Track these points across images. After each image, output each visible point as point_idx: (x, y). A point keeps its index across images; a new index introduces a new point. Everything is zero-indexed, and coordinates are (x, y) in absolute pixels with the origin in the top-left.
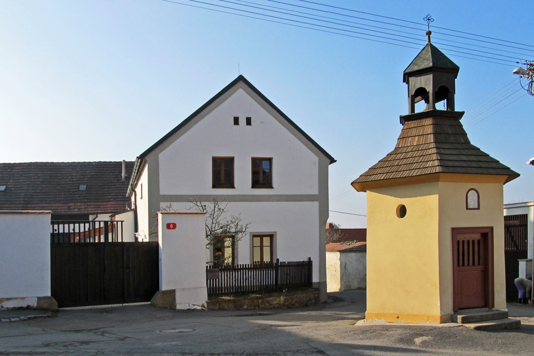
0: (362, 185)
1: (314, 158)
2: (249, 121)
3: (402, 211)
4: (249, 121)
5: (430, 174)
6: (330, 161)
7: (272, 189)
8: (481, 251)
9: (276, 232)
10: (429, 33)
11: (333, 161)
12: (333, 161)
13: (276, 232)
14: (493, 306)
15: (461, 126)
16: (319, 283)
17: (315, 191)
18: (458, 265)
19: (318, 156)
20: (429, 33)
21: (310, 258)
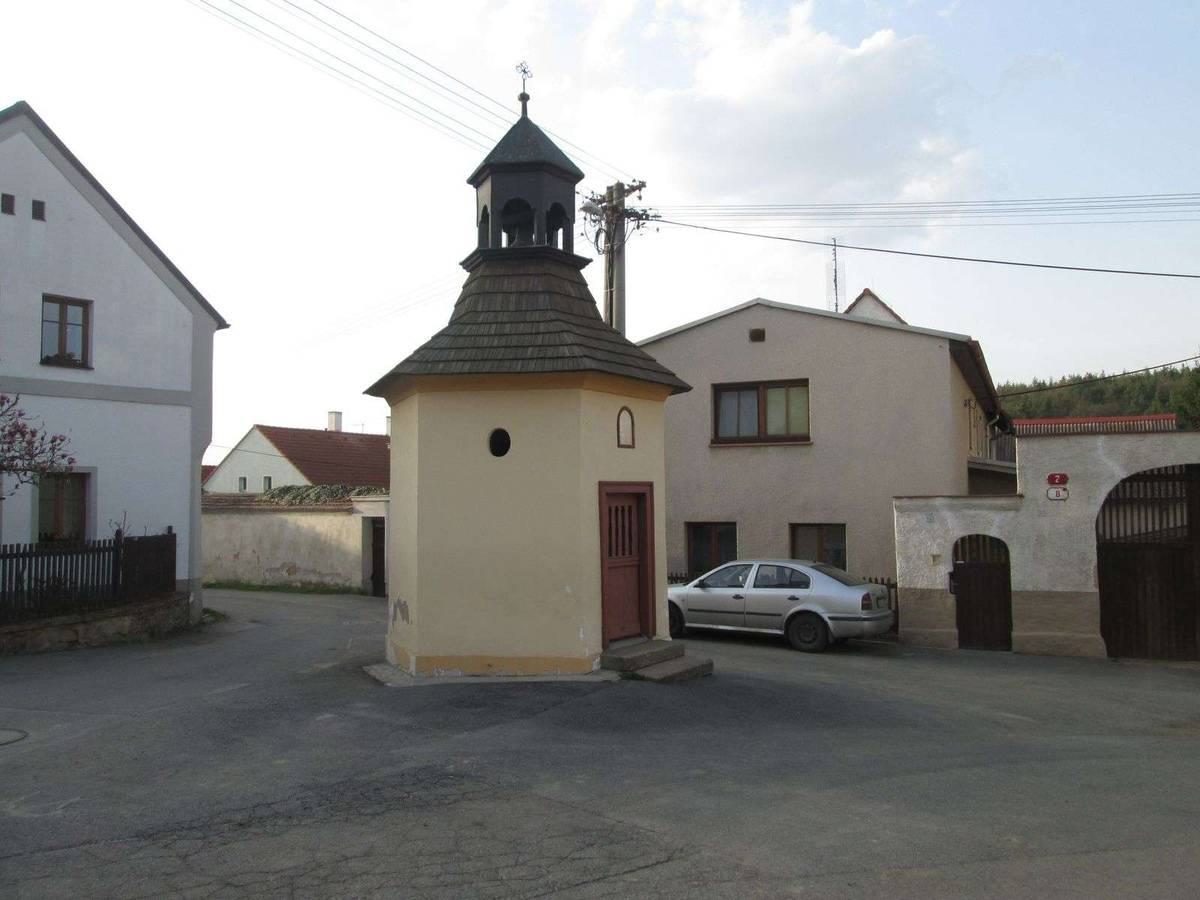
0: (683, 388)
1: (185, 314)
2: (38, 211)
3: (500, 443)
4: (38, 211)
5: (460, 373)
6: (217, 326)
7: (90, 372)
8: (374, 499)
9: (95, 469)
10: (524, 98)
11: (222, 324)
12: (222, 324)
13: (95, 469)
14: (654, 634)
15: (584, 285)
16: (189, 580)
17: (183, 384)
18: (610, 555)
19: (190, 310)
20: (524, 98)
21: (170, 528)
